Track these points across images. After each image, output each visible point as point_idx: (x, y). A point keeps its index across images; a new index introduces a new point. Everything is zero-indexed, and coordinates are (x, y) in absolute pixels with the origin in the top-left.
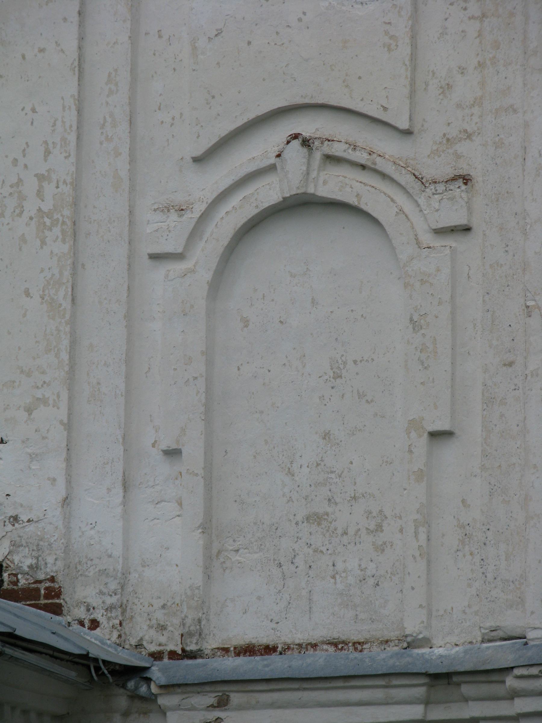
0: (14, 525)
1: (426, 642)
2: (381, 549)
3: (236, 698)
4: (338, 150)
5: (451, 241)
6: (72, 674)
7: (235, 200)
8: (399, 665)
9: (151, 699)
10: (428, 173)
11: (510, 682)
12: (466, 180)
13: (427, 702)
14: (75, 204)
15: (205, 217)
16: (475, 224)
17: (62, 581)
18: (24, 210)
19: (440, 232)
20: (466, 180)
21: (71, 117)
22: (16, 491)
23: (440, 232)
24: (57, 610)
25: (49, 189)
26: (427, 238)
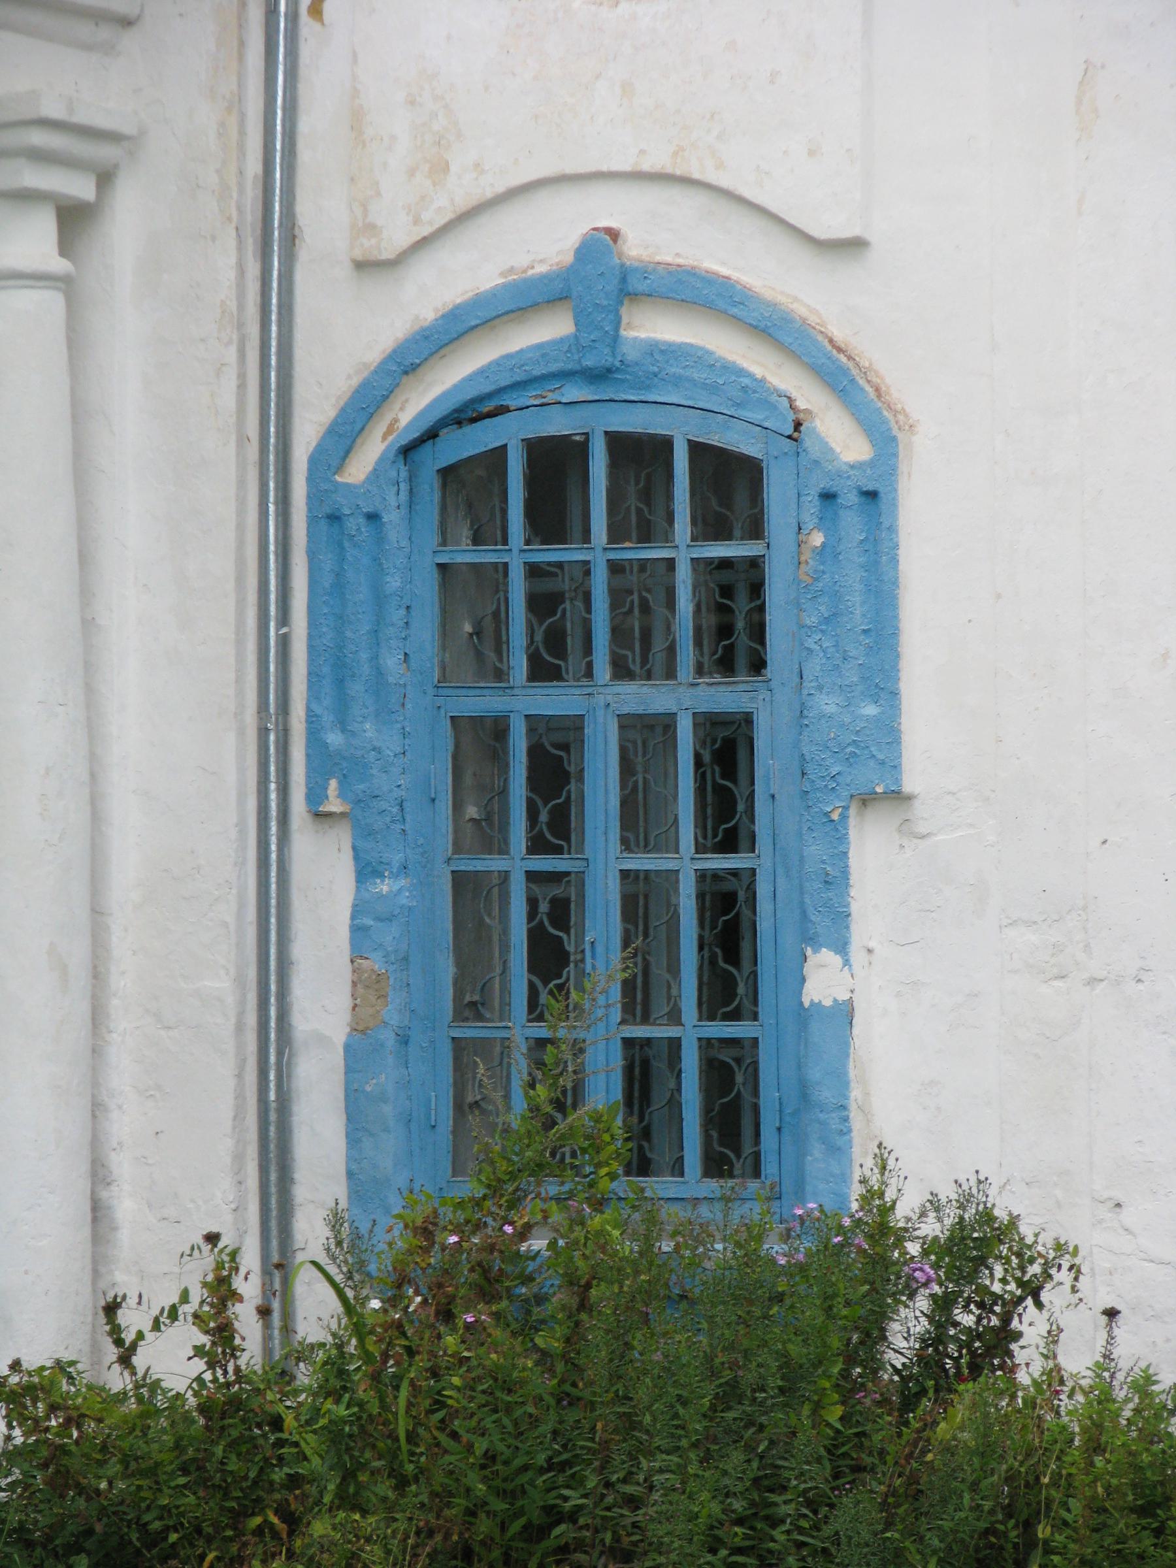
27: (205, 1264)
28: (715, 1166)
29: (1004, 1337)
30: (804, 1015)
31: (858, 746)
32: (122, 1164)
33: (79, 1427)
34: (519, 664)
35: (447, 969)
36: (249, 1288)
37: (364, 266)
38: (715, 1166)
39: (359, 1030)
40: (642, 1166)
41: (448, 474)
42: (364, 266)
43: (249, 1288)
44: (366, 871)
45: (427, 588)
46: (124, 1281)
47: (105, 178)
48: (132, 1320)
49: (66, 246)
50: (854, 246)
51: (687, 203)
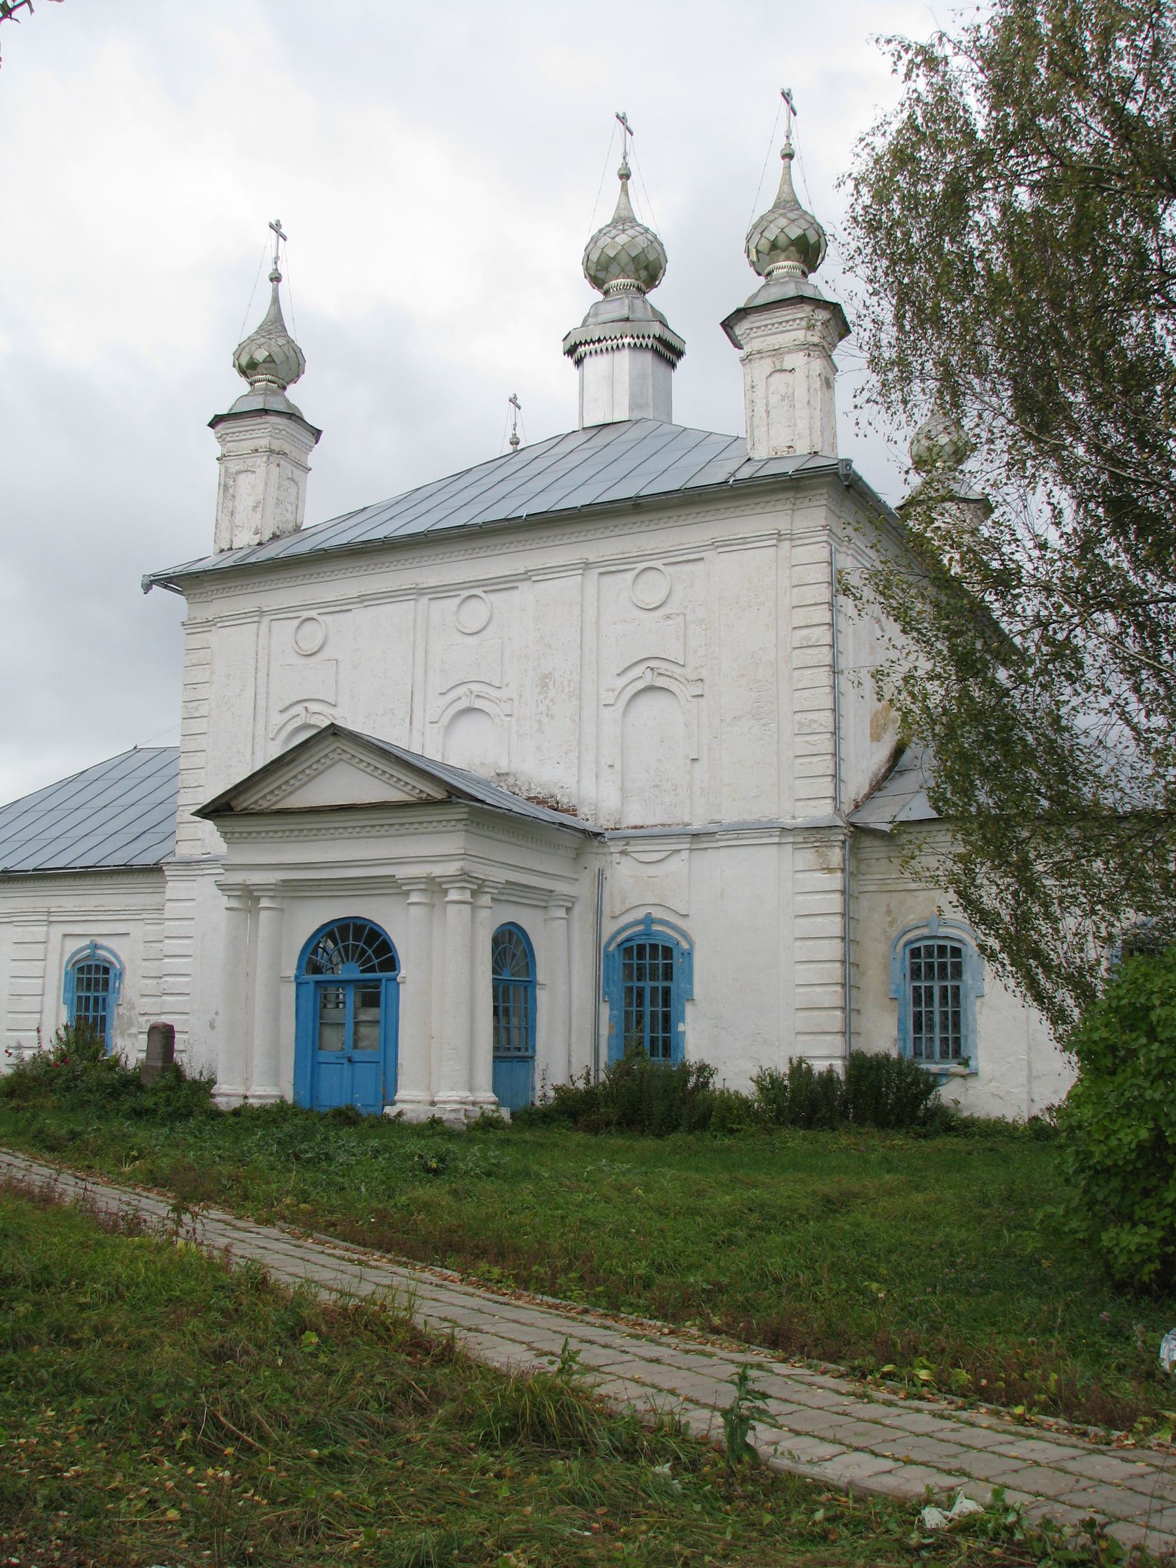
0: (747, 1299)
1: (690, 824)
2: (676, 795)
3: (632, 842)
4: (662, 671)
5: (698, 699)
6: (580, 835)
7: (629, 688)
8: (683, 831)
9: (604, 843)
10: (690, 678)
11: (717, 836)
12: (702, 680)
13: (691, 843)
14: (580, 689)
15: (620, 693)
16: (705, 694)
17: (578, 807)
18: (475, 1563)
19: (694, 696)
20: (702, 680)
21: (578, 662)
22: (888, 905)
23: (694, 696)
24: (575, 815)
25: (572, 684)
26: (690, 699)
27: (585, 1071)
28: (664, 1056)
29: (707, 1083)
30: (678, 1033)
31: (577, 1396)
32: (573, 1054)
33: (1096, 480)
34: (635, 978)
35: (623, 1024)
36: (592, 1073)
37: (612, 917)
38: (664, 1056)
39: (610, 1034)
40: (652, 1055)
41: (625, 949)
42: (612, 917)
43: (592, 1073)
44: (611, 1010)
45: (621, 967)
46: (573, 1072)
47: (573, 903)
48: (574, 1078)
49: (472, 896)
50: (687, 915)
51: (661, 909)
